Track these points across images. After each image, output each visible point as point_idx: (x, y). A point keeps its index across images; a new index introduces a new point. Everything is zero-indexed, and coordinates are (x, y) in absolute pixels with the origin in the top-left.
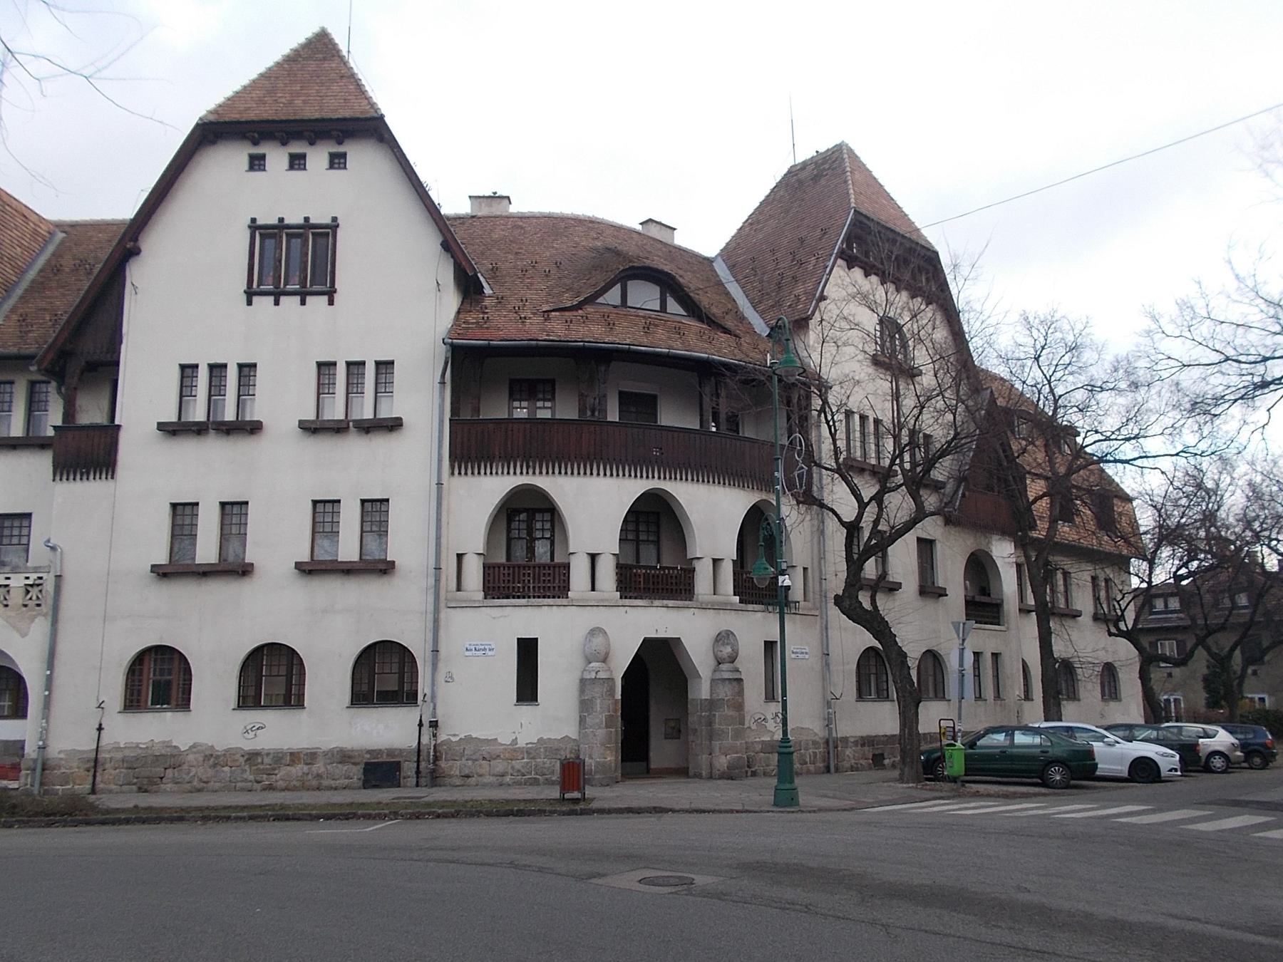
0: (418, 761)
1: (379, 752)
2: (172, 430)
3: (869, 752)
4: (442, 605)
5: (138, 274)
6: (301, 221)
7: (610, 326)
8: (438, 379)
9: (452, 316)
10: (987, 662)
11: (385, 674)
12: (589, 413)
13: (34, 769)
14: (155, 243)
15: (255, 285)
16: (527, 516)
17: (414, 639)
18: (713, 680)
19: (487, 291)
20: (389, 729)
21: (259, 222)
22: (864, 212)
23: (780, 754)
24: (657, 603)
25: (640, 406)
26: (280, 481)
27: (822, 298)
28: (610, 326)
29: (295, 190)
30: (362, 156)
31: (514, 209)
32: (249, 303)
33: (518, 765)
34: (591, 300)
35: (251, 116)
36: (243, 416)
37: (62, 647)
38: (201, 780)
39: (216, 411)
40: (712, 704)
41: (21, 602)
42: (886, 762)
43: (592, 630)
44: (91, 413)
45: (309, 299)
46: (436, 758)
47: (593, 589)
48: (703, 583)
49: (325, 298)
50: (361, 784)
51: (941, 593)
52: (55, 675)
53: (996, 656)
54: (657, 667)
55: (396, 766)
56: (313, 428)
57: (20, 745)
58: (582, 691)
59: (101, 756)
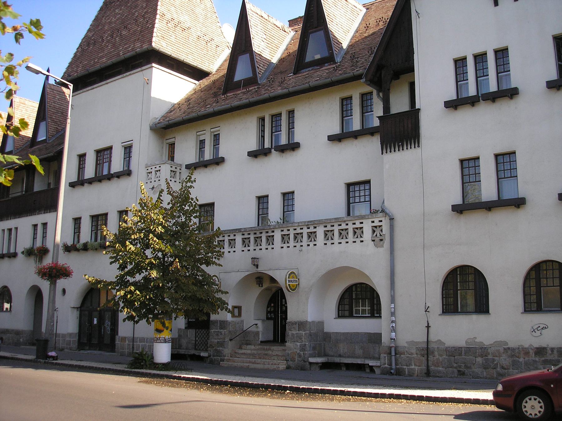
10: (40, 228)
23: (135, 358)
36: (461, 95)
37: (399, 268)
38: (503, 368)
44: (399, 105)
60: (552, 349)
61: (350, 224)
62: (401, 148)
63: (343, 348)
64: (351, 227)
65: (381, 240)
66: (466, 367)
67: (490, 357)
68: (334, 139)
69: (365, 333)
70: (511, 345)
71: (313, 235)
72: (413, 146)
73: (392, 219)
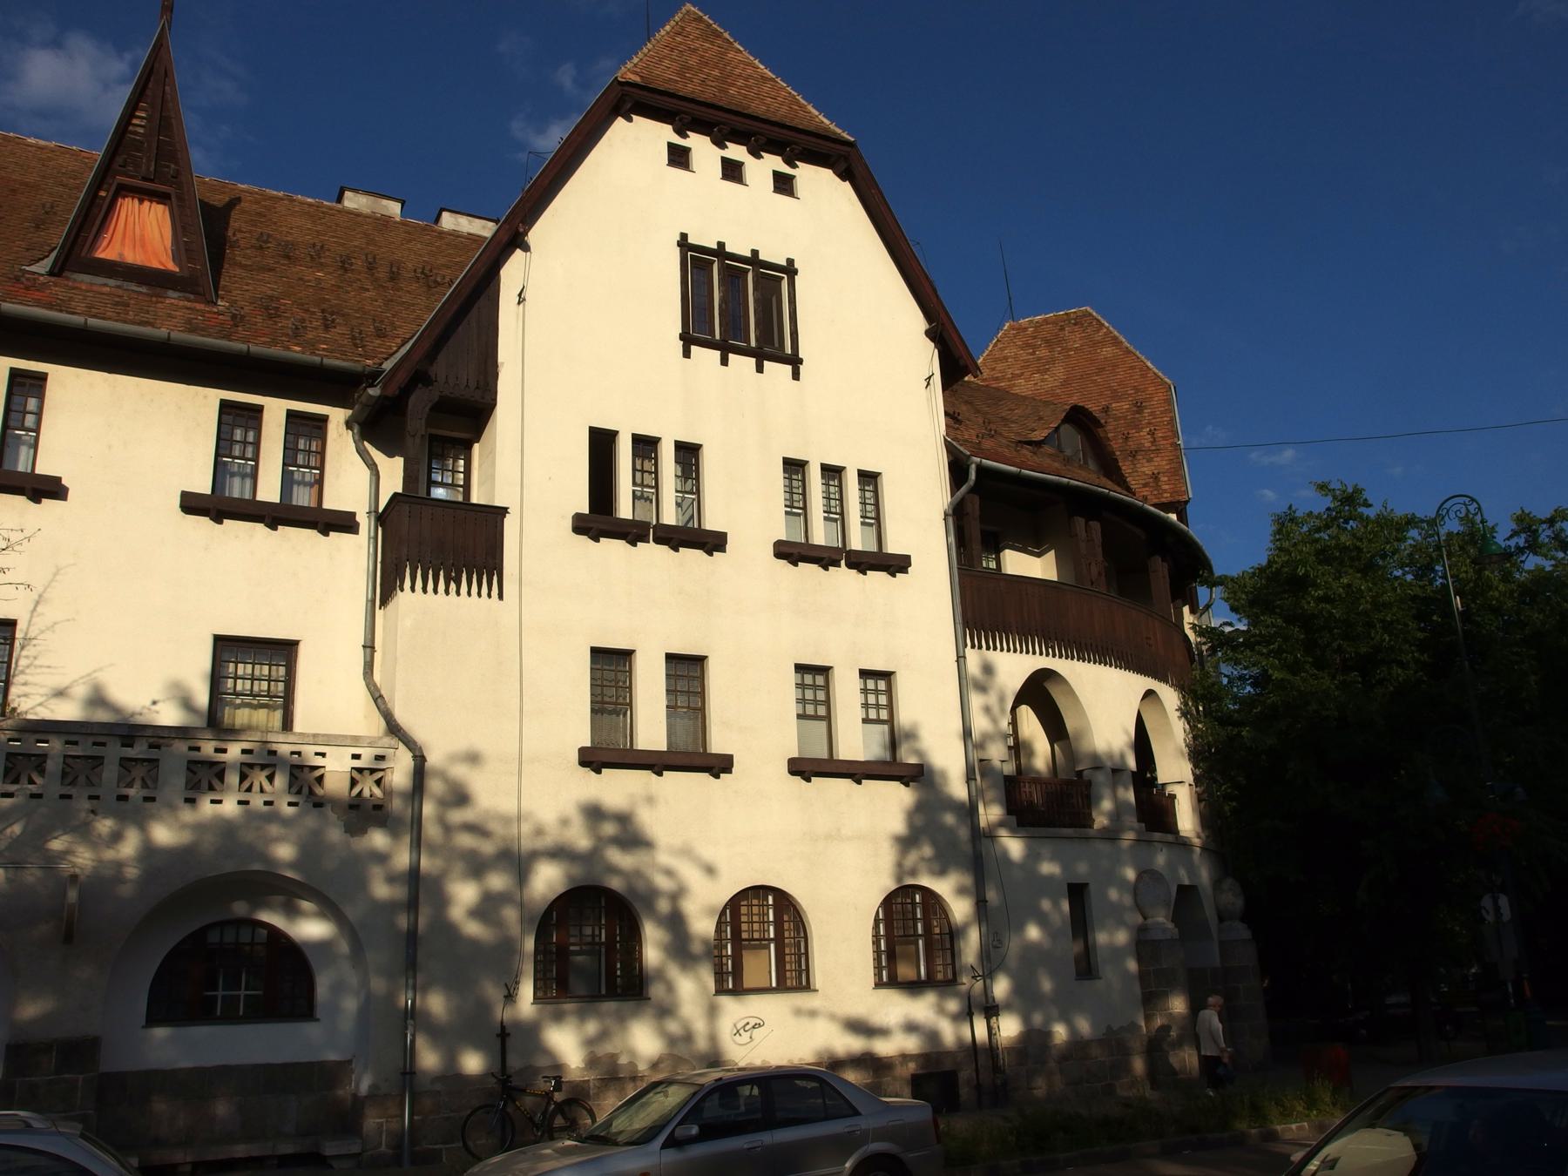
26: (750, 620)
32: (687, 354)
68: (192, 504)
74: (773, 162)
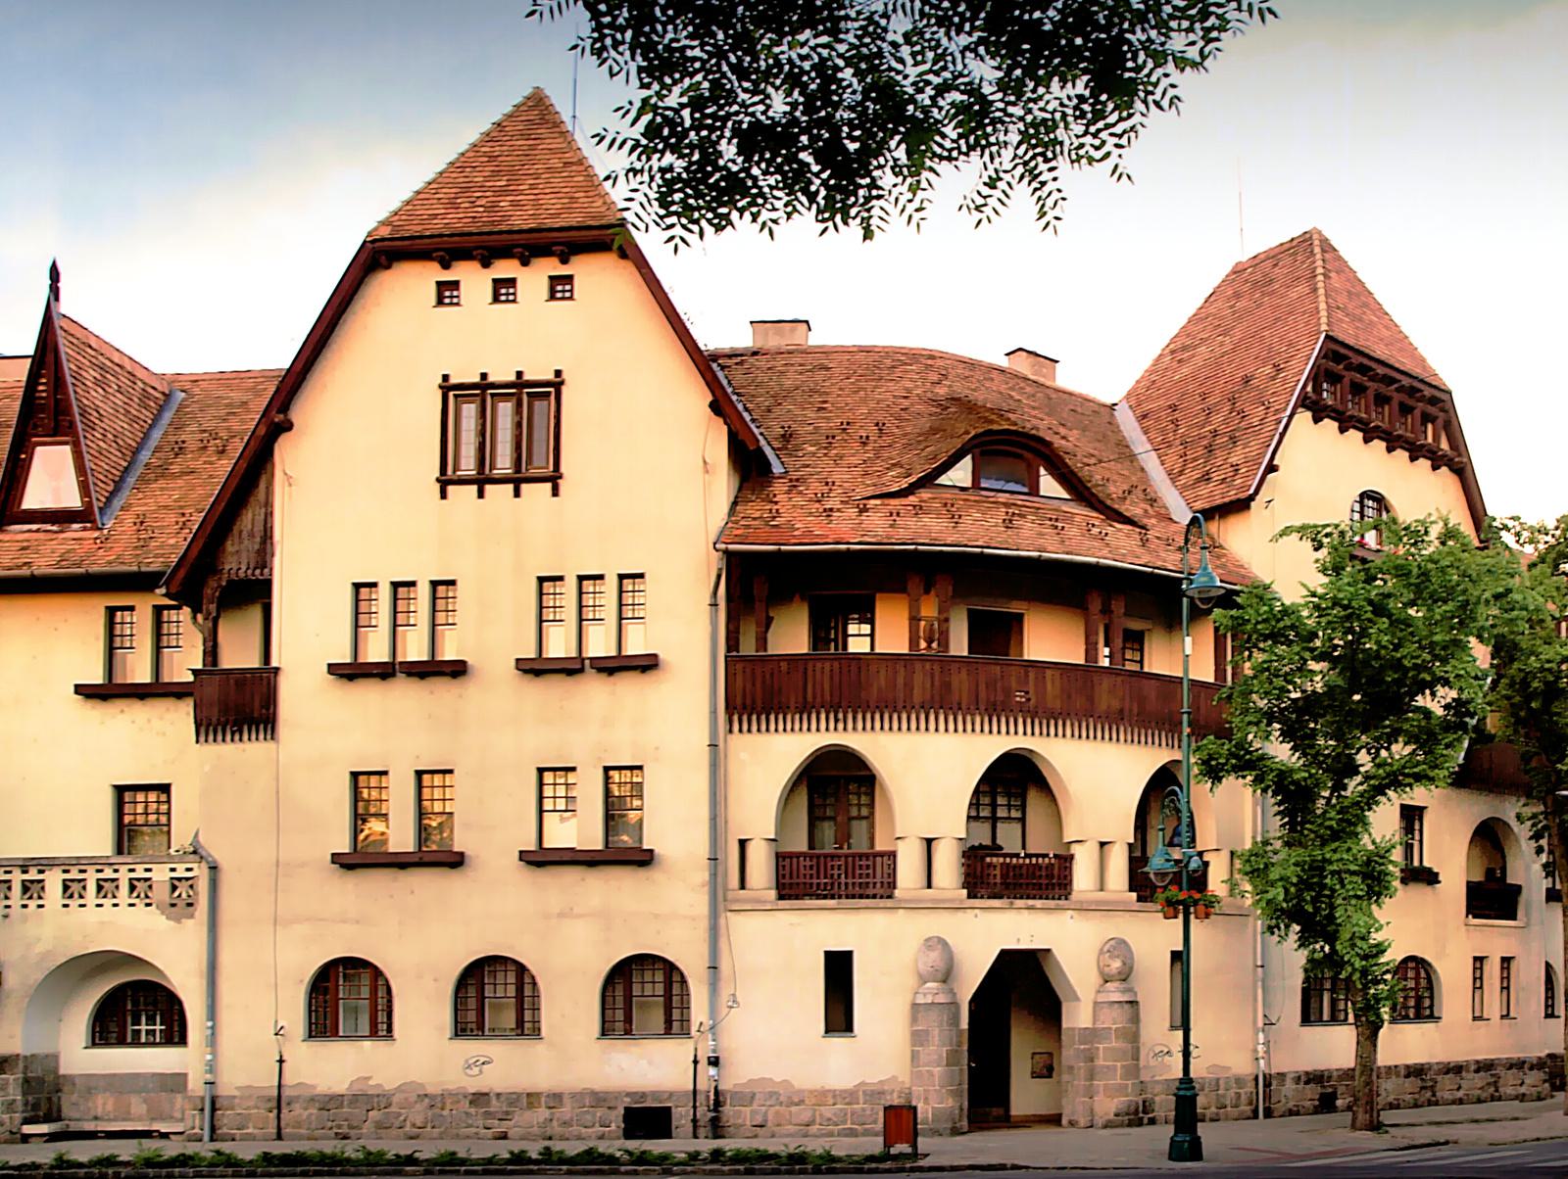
0: (695, 1107)
1: (643, 1095)
2: (350, 672)
3: (1313, 1091)
4: (721, 906)
5: (288, 454)
6: (512, 378)
7: (955, 519)
8: (707, 599)
9: (725, 508)
10: (1493, 970)
11: (642, 993)
12: (923, 644)
13: (202, 1110)
14: (320, 413)
15: (450, 471)
16: (836, 786)
17: (686, 952)
18: (1096, 1003)
19: (777, 468)
20: (654, 1067)
21: (453, 380)
22: (1341, 337)
24: (1019, 903)
25: (996, 635)
26: (494, 748)
27: (1272, 468)
28: (955, 519)
29: (502, 328)
30: (594, 275)
31: (815, 339)
32: (444, 495)
33: (828, 1111)
34: (928, 481)
35: (437, 226)
37: (225, 957)
38: (413, 1125)
39: (404, 658)
40: (1092, 1035)
41: (168, 900)
42: (1339, 1103)
43: (922, 943)
44: (239, 654)
45: (524, 487)
46: (718, 1103)
47: (929, 886)
48: (1083, 877)
49: (548, 486)
50: (621, 1132)
51: (1429, 877)
52: (218, 1025)
53: (1506, 961)
54: (1021, 986)
55: (664, 1114)
56: (535, 668)
57: (182, 1078)
58: (914, 1020)
59: (286, 1093)
60: (498, 1095)
61: (123, 869)
62: (237, 737)
63: (103, 1103)
64: (124, 876)
65: (190, 905)
66: (351, 1127)
67: (393, 1109)
68: (85, 691)
69: (154, 1075)
70: (430, 1090)
71: (35, 887)
72: (261, 736)
73: (214, 868)
74: (550, 267)
